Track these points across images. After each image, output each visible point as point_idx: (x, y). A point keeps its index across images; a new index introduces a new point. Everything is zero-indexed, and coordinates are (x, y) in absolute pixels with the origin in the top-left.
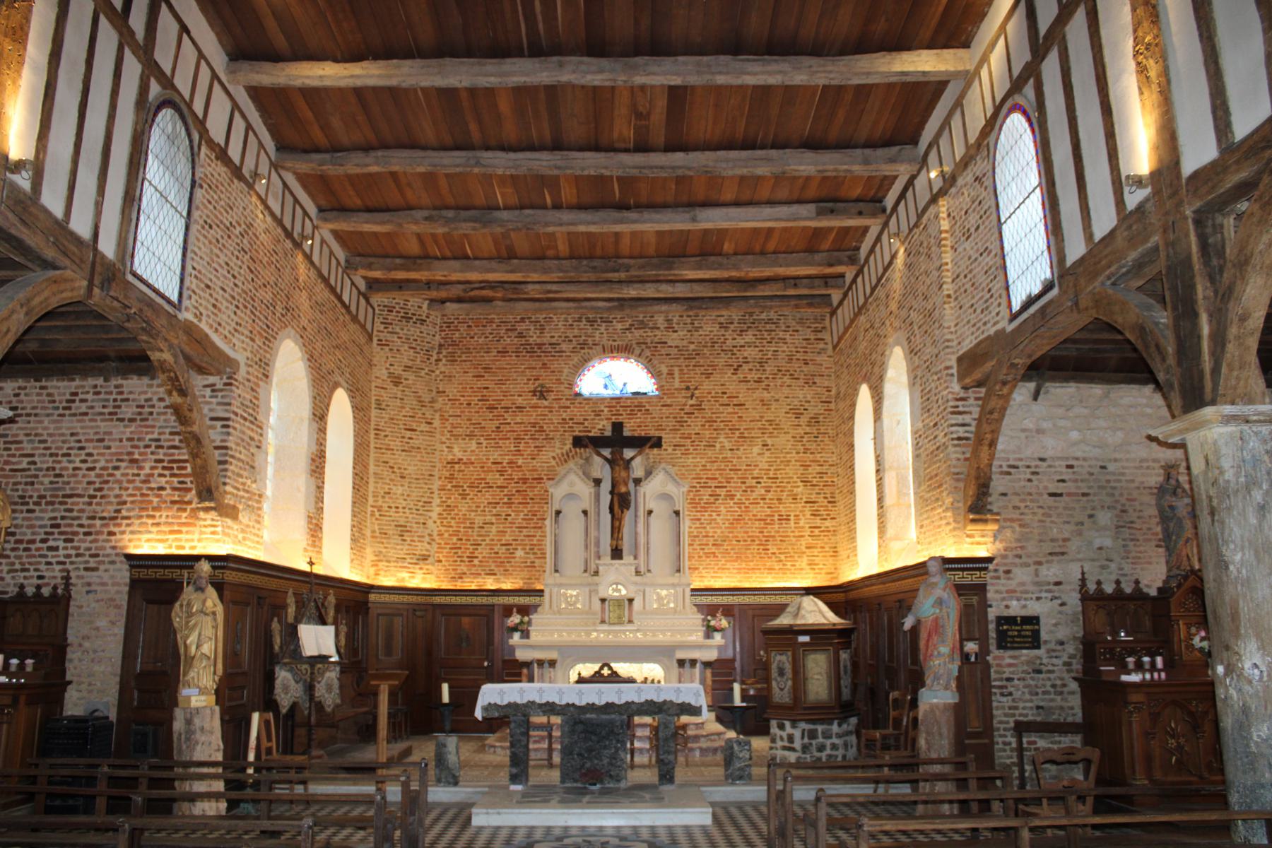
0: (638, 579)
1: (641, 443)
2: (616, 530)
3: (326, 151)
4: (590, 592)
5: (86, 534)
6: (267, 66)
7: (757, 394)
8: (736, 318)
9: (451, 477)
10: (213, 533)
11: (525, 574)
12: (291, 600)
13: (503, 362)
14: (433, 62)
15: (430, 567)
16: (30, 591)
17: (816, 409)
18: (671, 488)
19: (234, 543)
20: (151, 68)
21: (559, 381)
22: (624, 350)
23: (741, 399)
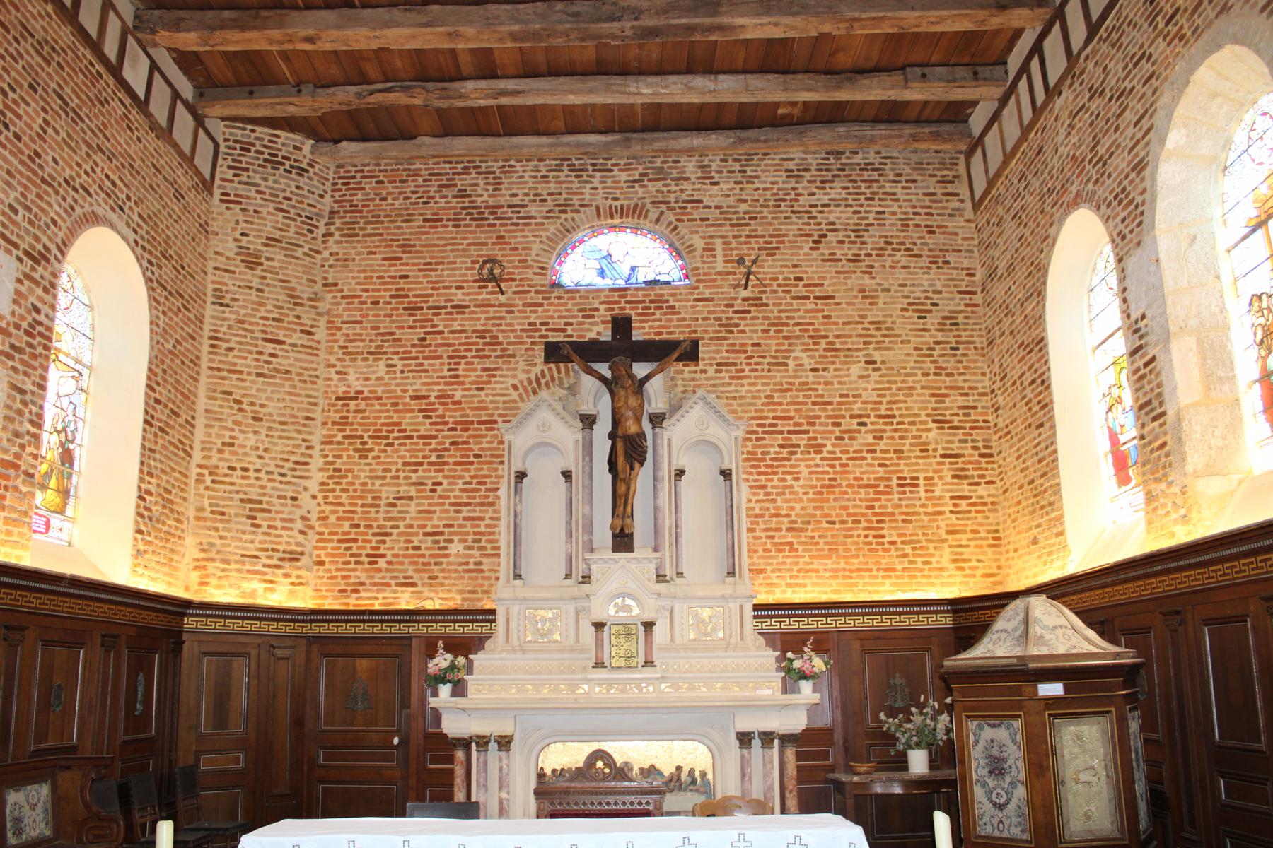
0: (662, 587)
1: (659, 351)
2: (621, 501)
4: (577, 612)
7: (854, 281)
8: (813, 161)
9: (343, 423)
11: (466, 584)
13: (433, 237)
15: (303, 573)
17: (951, 303)
18: (716, 431)
22: (627, 214)
23: (828, 289)
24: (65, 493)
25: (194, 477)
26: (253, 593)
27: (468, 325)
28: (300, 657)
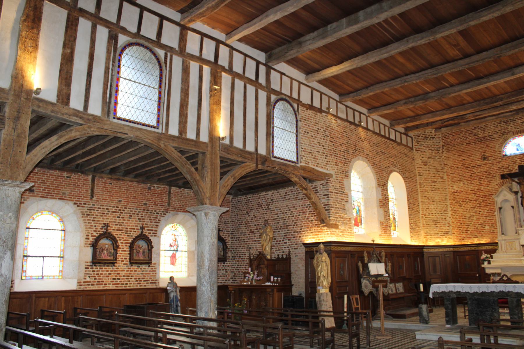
3: (354, 92)
5: (294, 237)
6: (316, 74)
9: (454, 199)
10: (328, 234)
11: (491, 236)
12: (365, 255)
14: (365, 55)
16: (280, 256)
19: (337, 237)
20: (270, 91)
21: (495, 152)
24: (395, 226)
25: (421, 217)
26: (438, 242)
27: (482, 170)
28: (452, 256)
